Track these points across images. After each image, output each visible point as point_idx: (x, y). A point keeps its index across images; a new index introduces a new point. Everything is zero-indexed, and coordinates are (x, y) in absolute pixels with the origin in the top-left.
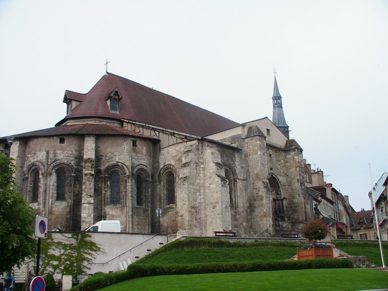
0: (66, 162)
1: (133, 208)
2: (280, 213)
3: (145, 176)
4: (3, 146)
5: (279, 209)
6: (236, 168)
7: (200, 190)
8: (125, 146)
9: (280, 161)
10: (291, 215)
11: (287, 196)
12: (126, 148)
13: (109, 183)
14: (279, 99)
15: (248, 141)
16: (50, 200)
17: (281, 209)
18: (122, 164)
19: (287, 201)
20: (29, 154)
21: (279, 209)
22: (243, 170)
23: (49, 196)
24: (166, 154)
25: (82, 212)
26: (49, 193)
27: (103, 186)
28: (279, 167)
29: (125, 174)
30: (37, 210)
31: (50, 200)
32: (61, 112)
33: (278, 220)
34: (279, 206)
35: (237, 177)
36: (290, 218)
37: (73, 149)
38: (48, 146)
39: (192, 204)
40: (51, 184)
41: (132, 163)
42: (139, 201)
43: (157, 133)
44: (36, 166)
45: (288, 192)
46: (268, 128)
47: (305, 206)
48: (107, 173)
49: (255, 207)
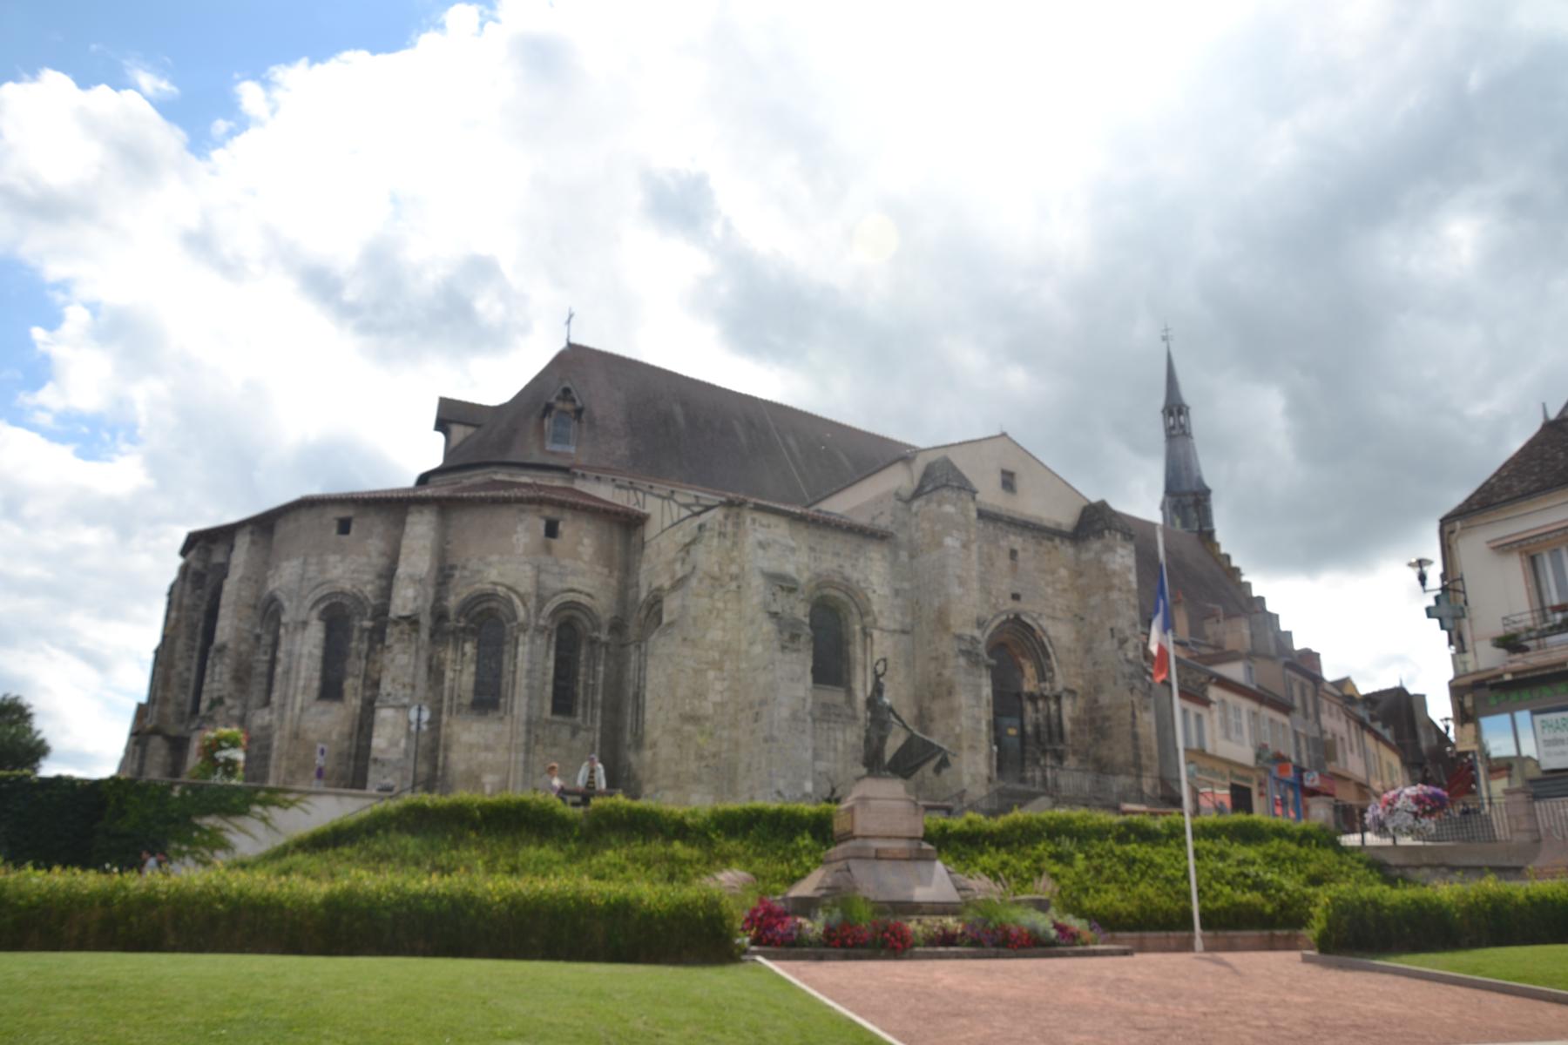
1: (530, 723)
2: (1050, 740)
3: (588, 624)
5: (1049, 726)
6: (870, 595)
9: (1053, 572)
13: (469, 648)
14: (1180, 412)
16: (299, 699)
17: (1055, 728)
18: (510, 588)
19: (1081, 702)
21: (1049, 726)
22: (899, 601)
23: (296, 688)
26: (297, 679)
28: (1050, 590)
29: (515, 618)
34: (1048, 717)
35: (875, 621)
40: (305, 651)
41: (539, 584)
42: (564, 702)
46: (1010, 468)
47: (1134, 715)
49: (932, 720)
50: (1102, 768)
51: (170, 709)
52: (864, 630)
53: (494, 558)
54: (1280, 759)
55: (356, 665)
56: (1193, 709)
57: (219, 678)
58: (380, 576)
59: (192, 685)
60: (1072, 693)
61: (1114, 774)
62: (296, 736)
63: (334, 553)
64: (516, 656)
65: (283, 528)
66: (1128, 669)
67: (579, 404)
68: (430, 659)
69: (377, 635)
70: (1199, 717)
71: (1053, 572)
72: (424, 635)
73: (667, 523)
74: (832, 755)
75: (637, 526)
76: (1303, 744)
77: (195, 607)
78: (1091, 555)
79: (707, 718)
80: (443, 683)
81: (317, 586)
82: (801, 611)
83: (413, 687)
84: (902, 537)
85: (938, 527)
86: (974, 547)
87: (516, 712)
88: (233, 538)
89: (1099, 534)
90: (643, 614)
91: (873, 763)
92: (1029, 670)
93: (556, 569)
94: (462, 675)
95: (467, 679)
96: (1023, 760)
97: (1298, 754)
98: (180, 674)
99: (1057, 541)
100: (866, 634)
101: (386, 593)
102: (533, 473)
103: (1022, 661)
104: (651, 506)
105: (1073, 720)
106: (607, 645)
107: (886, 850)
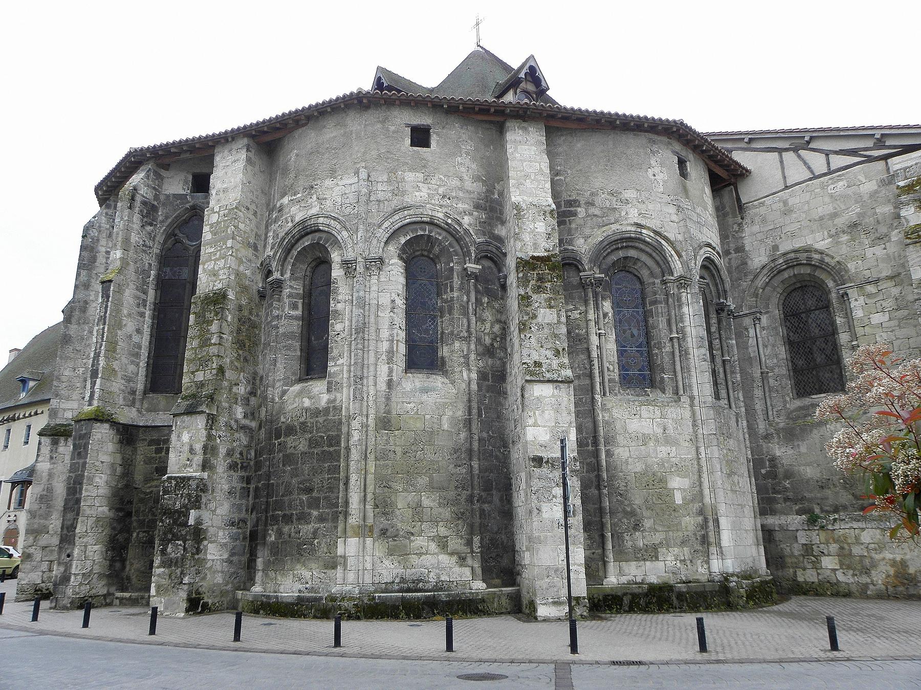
0: (441, 215)
4: (186, 182)
13: (607, 306)
18: (655, 232)
20: (283, 197)
25: (531, 421)
26: (378, 340)
30: (326, 411)
31: (384, 369)
37: (463, 169)
38: (365, 153)
40: (385, 300)
44: (317, 235)
48: (599, 267)
51: (117, 385)
62: (385, 423)
63: (412, 169)
81: (395, 211)
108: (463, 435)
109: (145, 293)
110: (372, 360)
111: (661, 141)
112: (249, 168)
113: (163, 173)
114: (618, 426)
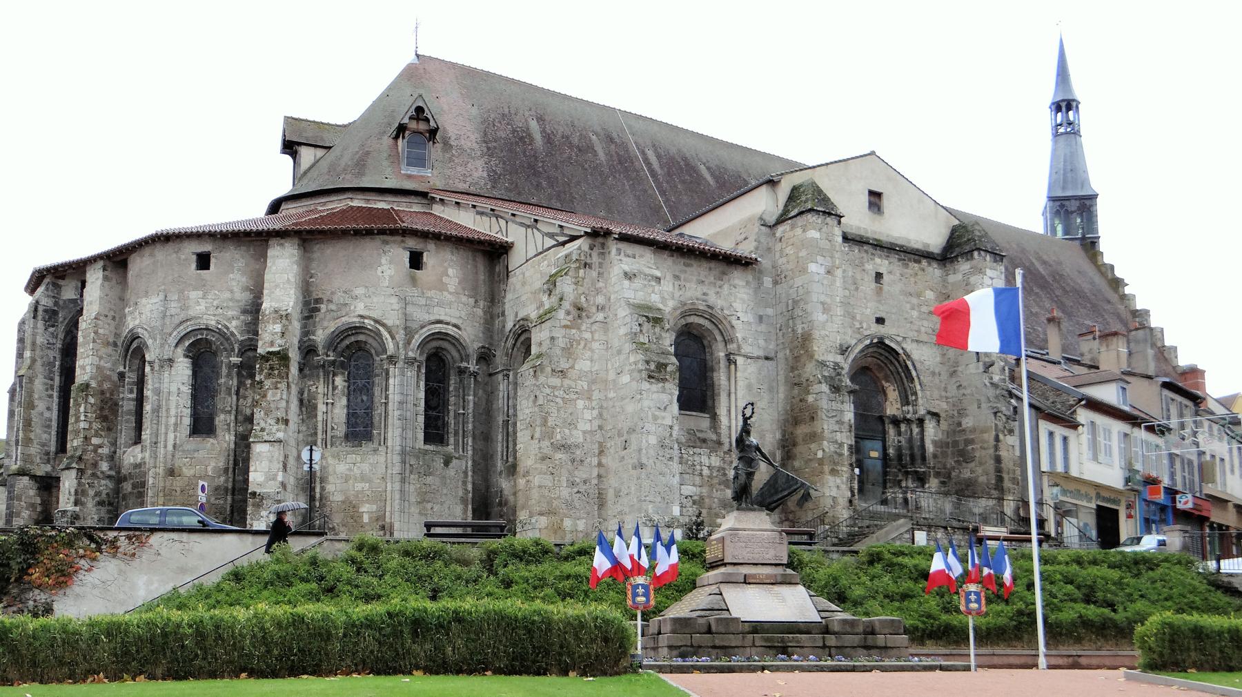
0: (213, 323)
5: (911, 448)
6: (734, 322)
7: (590, 391)
8: (385, 268)
9: (919, 295)
10: (953, 468)
11: (941, 407)
12: (388, 273)
13: (339, 381)
14: (1069, 108)
15: (784, 232)
16: (171, 436)
18: (376, 321)
19: (944, 425)
21: (911, 448)
22: (763, 328)
24: (518, 286)
27: (321, 390)
29: (385, 350)
31: (171, 436)
32: (280, 177)
33: (904, 484)
34: (910, 440)
35: (739, 347)
36: (949, 477)
37: (234, 283)
39: (559, 437)
40: (174, 388)
42: (435, 431)
43: (503, 222)
45: (949, 394)
47: (997, 439)
49: (794, 445)
50: (965, 490)
51: (34, 450)
52: (728, 355)
53: (360, 291)
54: (1151, 482)
55: (225, 401)
56: (1059, 431)
57: (83, 416)
58: (244, 312)
59: (54, 424)
60: (935, 415)
61: (974, 495)
63: (195, 289)
64: (387, 389)
65: (137, 264)
66: (991, 392)
67: (432, 124)
68: (301, 393)
69: (246, 370)
70: (1065, 439)
71: (919, 295)
72: (294, 370)
73: (531, 253)
74: (698, 479)
75: (499, 256)
76: (1178, 465)
77: (50, 345)
78: (959, 277)
79: (577, 446)
80: (316, 416)
81: (181, 323)
82: (668, 341)
83: (286, 422)
84: (765, 262)
85: (803, 253)
86: (839, 273)
87: (389, 443)
88: (84, 273)
89: (968, 255)
90: (510, 342)
91: (742, 496)
92: (893, 394)
93: (423, 301)
94: (334, 408)
95: (340, 412)
96: (885, 482)
97: (1172, 476)
98: (42, 414)
99: (924, 262)
100: (730, 361)
101: (253, 328)
102: (390, 198)
103: (886, 385)
104: (513, 234)
105: (935, 443)
106: (475, 375)
107: (754, 576)
108: (222, 479)
109: (52, 379)
110: (163, 430)
111: (394, 242)
112: (106, 284)
113: (61, 282)
114: (331, 469)
